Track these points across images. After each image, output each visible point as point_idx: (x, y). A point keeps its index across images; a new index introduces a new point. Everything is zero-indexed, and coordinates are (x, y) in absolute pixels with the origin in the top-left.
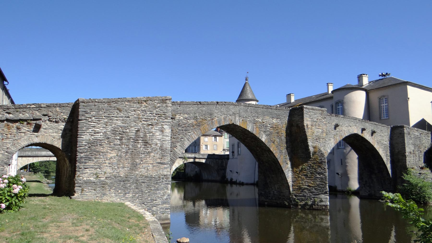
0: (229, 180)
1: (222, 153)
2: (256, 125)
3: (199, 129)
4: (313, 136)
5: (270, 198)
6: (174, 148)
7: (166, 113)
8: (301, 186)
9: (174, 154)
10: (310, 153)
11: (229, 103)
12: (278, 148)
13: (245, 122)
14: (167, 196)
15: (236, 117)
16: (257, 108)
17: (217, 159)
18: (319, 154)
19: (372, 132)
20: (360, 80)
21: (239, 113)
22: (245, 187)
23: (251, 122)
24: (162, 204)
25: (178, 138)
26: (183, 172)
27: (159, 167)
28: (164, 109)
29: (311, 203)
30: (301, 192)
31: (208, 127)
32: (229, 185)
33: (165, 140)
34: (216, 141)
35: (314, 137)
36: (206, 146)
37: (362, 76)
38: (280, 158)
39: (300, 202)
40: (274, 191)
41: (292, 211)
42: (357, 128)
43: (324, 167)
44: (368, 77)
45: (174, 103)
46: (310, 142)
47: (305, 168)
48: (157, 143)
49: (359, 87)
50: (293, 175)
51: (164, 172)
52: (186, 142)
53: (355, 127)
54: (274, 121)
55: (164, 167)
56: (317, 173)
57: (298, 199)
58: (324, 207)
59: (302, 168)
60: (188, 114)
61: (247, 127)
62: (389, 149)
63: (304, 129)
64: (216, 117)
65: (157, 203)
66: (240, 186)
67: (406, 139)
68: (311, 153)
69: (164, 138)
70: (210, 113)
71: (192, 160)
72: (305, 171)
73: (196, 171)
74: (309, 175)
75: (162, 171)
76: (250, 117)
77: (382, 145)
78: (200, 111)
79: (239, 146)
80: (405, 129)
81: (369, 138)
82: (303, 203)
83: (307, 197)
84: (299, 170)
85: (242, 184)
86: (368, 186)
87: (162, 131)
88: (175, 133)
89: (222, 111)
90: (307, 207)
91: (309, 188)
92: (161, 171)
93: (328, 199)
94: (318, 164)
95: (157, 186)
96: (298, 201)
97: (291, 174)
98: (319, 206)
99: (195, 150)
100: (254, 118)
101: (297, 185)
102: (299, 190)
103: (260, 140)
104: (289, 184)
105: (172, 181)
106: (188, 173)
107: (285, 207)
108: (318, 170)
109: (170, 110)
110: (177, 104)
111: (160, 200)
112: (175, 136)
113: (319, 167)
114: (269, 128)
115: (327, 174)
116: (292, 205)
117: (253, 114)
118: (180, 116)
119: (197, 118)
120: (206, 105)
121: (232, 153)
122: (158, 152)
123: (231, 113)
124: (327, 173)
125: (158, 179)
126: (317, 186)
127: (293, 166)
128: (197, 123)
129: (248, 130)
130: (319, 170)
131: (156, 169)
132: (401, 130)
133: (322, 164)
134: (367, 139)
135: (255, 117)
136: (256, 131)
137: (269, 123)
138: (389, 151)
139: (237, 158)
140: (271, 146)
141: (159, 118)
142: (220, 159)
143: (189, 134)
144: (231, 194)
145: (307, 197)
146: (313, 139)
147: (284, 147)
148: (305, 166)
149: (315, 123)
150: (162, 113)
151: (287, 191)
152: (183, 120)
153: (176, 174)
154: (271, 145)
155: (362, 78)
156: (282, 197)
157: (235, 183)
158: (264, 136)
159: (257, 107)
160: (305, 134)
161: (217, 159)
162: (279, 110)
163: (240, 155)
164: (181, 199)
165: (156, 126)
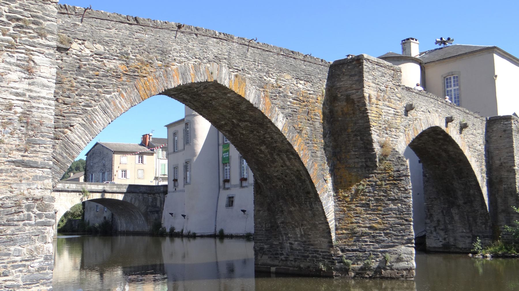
0: (168, 230)
1: (154, 183)
2: (264, 91)
3: (132, 85)
4: (379, 122)
5: (283, 257)
6: (66, 130)
7: (41, 21)
8: (355, 228)
9: (65, 146)
10: (374, 156)
11: (207, 33)
12: (308, 147)
13: (242, 81)
14: (42, 259)
15: (221, 66)
16: (267, 53)
17: (145, 193)
18: (394, 160)
19: (461, 127)
20: (407, 49)
21: (229, 59)
22: (198, 241)
23: (254, 82)
24: (27, 286)
25: (77, 103)
26: (79, 220)
27: (19, 174)
28: (36, 6)
29: (377, 264)
30: (355, 242)
31: (156, 84)
32: (168, 239)
33: (39, 97)
34: (142, 162)
35: (381, 123)
36: (124, 172)
37: (410, 42)
38: (311, 167)
39: (353, 264)
40: (293, 242)
41: (335, 282)
42: (439, 116)
43: (404, 186)
44: (418, 44)
45: (66, 8)
46: (374, 134)
47: (363, 190)
48: (13, 102)
49: (409, 59)
50: (337, 206)
51: (32, 191)
52: (100, 115)
53: (436, 114)
54: (301, 86)
55: (33, 174)
56: (389, 200)
57: (349, 258)
58: (405, 273)
59: (357, 191)
60: (104, 43)
61: (245, 93)
62: (485, 159)
63: (365, 105)
64: (175, 60)
65: (8, 283)
66: (190, 241)
67: (514, 141)
68: (377, 156)
69: (36, 92)
70: (161, 49)
71: (98, 196)
72: (363, 195)
73: (105, 218)
74: (373, 204)
75: (28, 187)
76: (252, 70)
77: (475, 152)
78: (137, 40)
79: (188, 168)
80: (513, 121)
81: (457, 138)
82: (361, 264)
83: (368, 251)
84: (350, 194)
85: (194, 236)
86: (442, 230)
87: (29, 70)
88: (69, 90)
89: (189, 49)
90: (368, 275)
91: (372, 232)
92: (24, 187)
93: (414, 255)
94: (392, 180)
95: (9, 232)
96: (349, 261)
97: (334, 204)
98: (395, 270)
99: (102, 179)
100: (261, 74)
101: (345, 227)
102: (351, 237)
103: (273, 124)
104: (330, 224)
105: (58, 235)
106: (89, 221)
107: (318, 274)
108: (392, 193)
109: (54, 12)
110: (74, 13)
111: (18, 274)
112: (69, 97)
113: (395, 187)
114: (291, 100)
115: (411, 201)
116: (336, 270)
117: (258, 66)
118: (82, 47)
119: (127, 58)
120: (150, 28)
121: (173, 182)
122: (14, 129)
123: (211, 57)
124: (412, 199)
125: (13, 211)
126: (390, 227)
127: (336, 188)
128: (127, 69)
129: (248, 99)
130: (393, 193)
131: (6, 181)
132: (506, 124)
133: (401, 180)
134: (454, 139)
135: (263, 72)
136: (264, 104)
137: (291, 90)
138: (484, 163)
139: (183, 191)
140: (295, 141)
141: (18, 29)
142: (150, 194)
143: (108, 96)
144: (172, 255)
145: (368, 251)
146: (380, 127)
147: (320, 145)
148: (363, 185)
149: (382, 94)
150: (28, 19)
151: (325, 240)
152: (91, 58)
153: (66, 223)
154: (294, 139)
155: (410, 45)
156: (310, 255)
157: (180, 235)
158: (281, 117)
159: (267, 49)
160: (365, 115)
161: (145, 193)
162: (309, 62)
163: (189, 184)
164: (75, 268)
165: (10, 52)
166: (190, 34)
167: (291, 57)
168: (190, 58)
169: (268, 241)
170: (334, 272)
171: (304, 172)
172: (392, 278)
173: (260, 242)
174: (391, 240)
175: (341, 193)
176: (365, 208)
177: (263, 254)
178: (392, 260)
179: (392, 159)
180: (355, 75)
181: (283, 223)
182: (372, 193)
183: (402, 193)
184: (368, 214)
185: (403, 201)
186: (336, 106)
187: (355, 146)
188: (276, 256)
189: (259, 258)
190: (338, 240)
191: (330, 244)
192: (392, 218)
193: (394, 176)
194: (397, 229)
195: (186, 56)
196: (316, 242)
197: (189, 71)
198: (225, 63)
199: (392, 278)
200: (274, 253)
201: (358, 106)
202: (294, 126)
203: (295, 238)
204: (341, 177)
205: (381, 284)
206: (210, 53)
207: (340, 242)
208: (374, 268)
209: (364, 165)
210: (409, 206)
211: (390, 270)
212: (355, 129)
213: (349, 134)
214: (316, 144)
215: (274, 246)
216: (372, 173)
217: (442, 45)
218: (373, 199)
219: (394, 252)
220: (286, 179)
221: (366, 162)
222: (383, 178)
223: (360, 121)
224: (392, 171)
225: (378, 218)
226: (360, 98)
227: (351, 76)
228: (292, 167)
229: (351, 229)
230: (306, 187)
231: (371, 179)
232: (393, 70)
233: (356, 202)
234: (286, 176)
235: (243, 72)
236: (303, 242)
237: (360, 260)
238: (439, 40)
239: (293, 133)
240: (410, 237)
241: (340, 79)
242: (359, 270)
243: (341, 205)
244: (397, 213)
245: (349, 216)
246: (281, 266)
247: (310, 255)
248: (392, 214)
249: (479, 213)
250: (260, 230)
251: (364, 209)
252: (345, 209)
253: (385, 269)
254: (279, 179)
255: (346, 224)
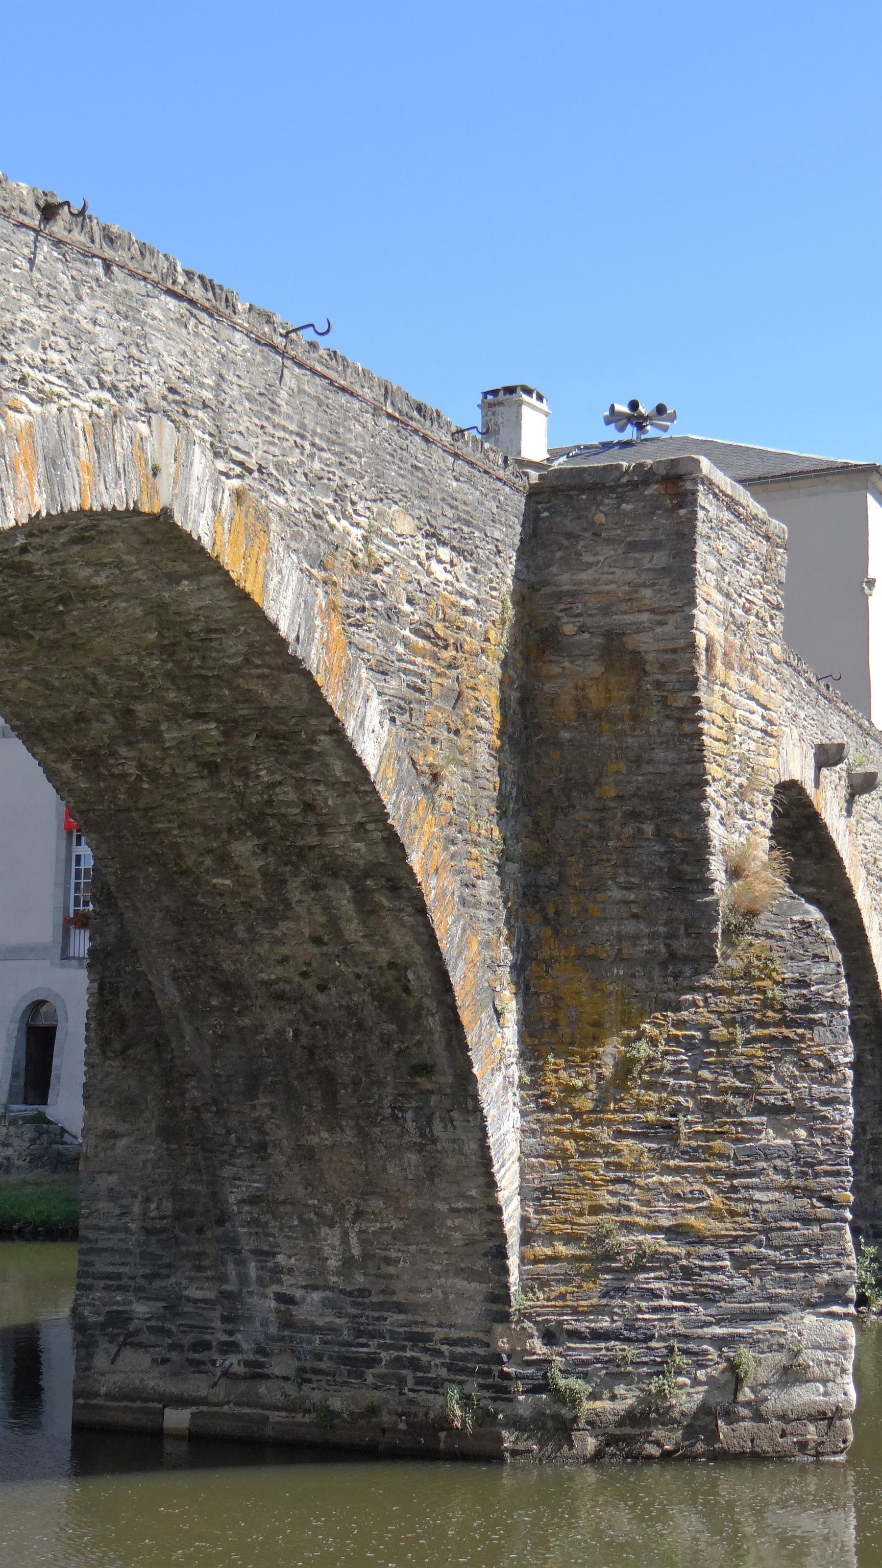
5: (233, 1361)
10: (709, 912)
16: (343, 399)
18: (784, 933)
29: (699, 1395)
30: (605, 1295)
37: (520, 404)
39: (594, 1396)
40: (298, 1294)
43: (825, 1049)
44: (547, 414)
47: (650, 1060)
50: (533, 1132)
56: (760, 1109)
57: (578, 1369)
58: (812, 1432)
59: (625, 1066)
72: (649, 1086)
83: (662, 1338)
84: (592, 1077)
90: (658, 1443)
91: (681, 1250)
94: (776, 1024)
96: (576, 1384)
98: (775, 1422)
100: (319, 498)
108: (772, 1078)
116: (517, 1424)
123: (156, 388)
124: (851, 1110)
126: (760, 1232)
133: (811, 1024)
137: (410, 588)
145: (662, 1338)
148: (653, 1042)
154: (413, 818)
156: (383, 1355)
160: (687, 728)
166: (87, 255)
167: (416, 431)
168: (81, 381)
169: (158, 1283)
170: (505, 1433)
171: (427, 976)
172: (757, 1457)
173: (107, 1288)
174: (763, 1288)
175: (555, 1071)
176: (654, 1146)
177: (124, 1344)
178: (763, 1375)
179: (776, 931)
180: (654, 545)
181: (253, 1200)
182: (687, 1077)
183: (813, 1080)
184: (668, 1170)
185: (815, 1118)
186: (550, 678)
187: (626, 865)
188: (197, 1356)
189: (101, 1362)
190: (532, 1289)
191: (495, 1307)
192: (768, 1189)
193: (784, 1007)
194: (789, 1238)
195: (69, 367)
196: (425, 1296)
197: (75, 445)
198: (203, 426)
199: (757, 1457)
200: (188, 1340)
201: (659, 685)
202: (415, 756)
203: (309, 1274)
204: (557, 1002)
205: (713, 1489)
206: (152, 370)
207: (541, 1295)
208: (683, 1414)
209: (663, 950)
210: (842, 1139)
211: (753, 1419)
212: (632, 788)
213: (604, 809)
214: (476, 844)
215: (188, 1308)
216: (693, 989)
217: (630, 433)
218: (691, 1104)
219: (774, 1341)
220: (321, 998)
221: (671, 936)
222: (740, 1010)
223: (660, 754)
224: (777, 983)
225: (710, 1192)
226: (674, 651)
227: (633, 546)
228: (368, 948)
229: (590, 1239)
230: (419, 1044)
231: (685, 1014)
232: (767, 538)
233: (619, 1117)
234: (322, 988)
235: (262, 481)
236: (350, 1294)
237: (624, 1377)
238: (622, 408)
239: (410, 793)
240: (840, 1274)
241: (579, 554)
242: (620, 1424)
243: (550, 1129)
244: (793, 1170)
245: (583, 1180)
246: (220, 1404)
247: (383, 1355)
248: (771, 1172)
249: (869, 1136)
250: (113, 1230)
251: (650, 1150)
252: (569, 1144)
253: (731, 1417)
254: (280, 996)
255: (570, 1216)
